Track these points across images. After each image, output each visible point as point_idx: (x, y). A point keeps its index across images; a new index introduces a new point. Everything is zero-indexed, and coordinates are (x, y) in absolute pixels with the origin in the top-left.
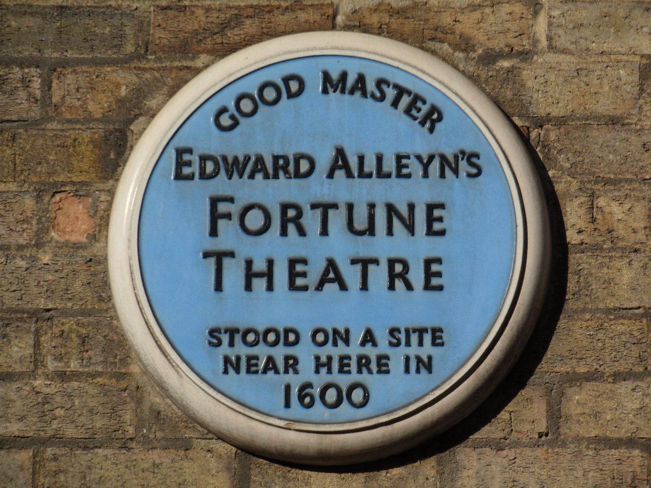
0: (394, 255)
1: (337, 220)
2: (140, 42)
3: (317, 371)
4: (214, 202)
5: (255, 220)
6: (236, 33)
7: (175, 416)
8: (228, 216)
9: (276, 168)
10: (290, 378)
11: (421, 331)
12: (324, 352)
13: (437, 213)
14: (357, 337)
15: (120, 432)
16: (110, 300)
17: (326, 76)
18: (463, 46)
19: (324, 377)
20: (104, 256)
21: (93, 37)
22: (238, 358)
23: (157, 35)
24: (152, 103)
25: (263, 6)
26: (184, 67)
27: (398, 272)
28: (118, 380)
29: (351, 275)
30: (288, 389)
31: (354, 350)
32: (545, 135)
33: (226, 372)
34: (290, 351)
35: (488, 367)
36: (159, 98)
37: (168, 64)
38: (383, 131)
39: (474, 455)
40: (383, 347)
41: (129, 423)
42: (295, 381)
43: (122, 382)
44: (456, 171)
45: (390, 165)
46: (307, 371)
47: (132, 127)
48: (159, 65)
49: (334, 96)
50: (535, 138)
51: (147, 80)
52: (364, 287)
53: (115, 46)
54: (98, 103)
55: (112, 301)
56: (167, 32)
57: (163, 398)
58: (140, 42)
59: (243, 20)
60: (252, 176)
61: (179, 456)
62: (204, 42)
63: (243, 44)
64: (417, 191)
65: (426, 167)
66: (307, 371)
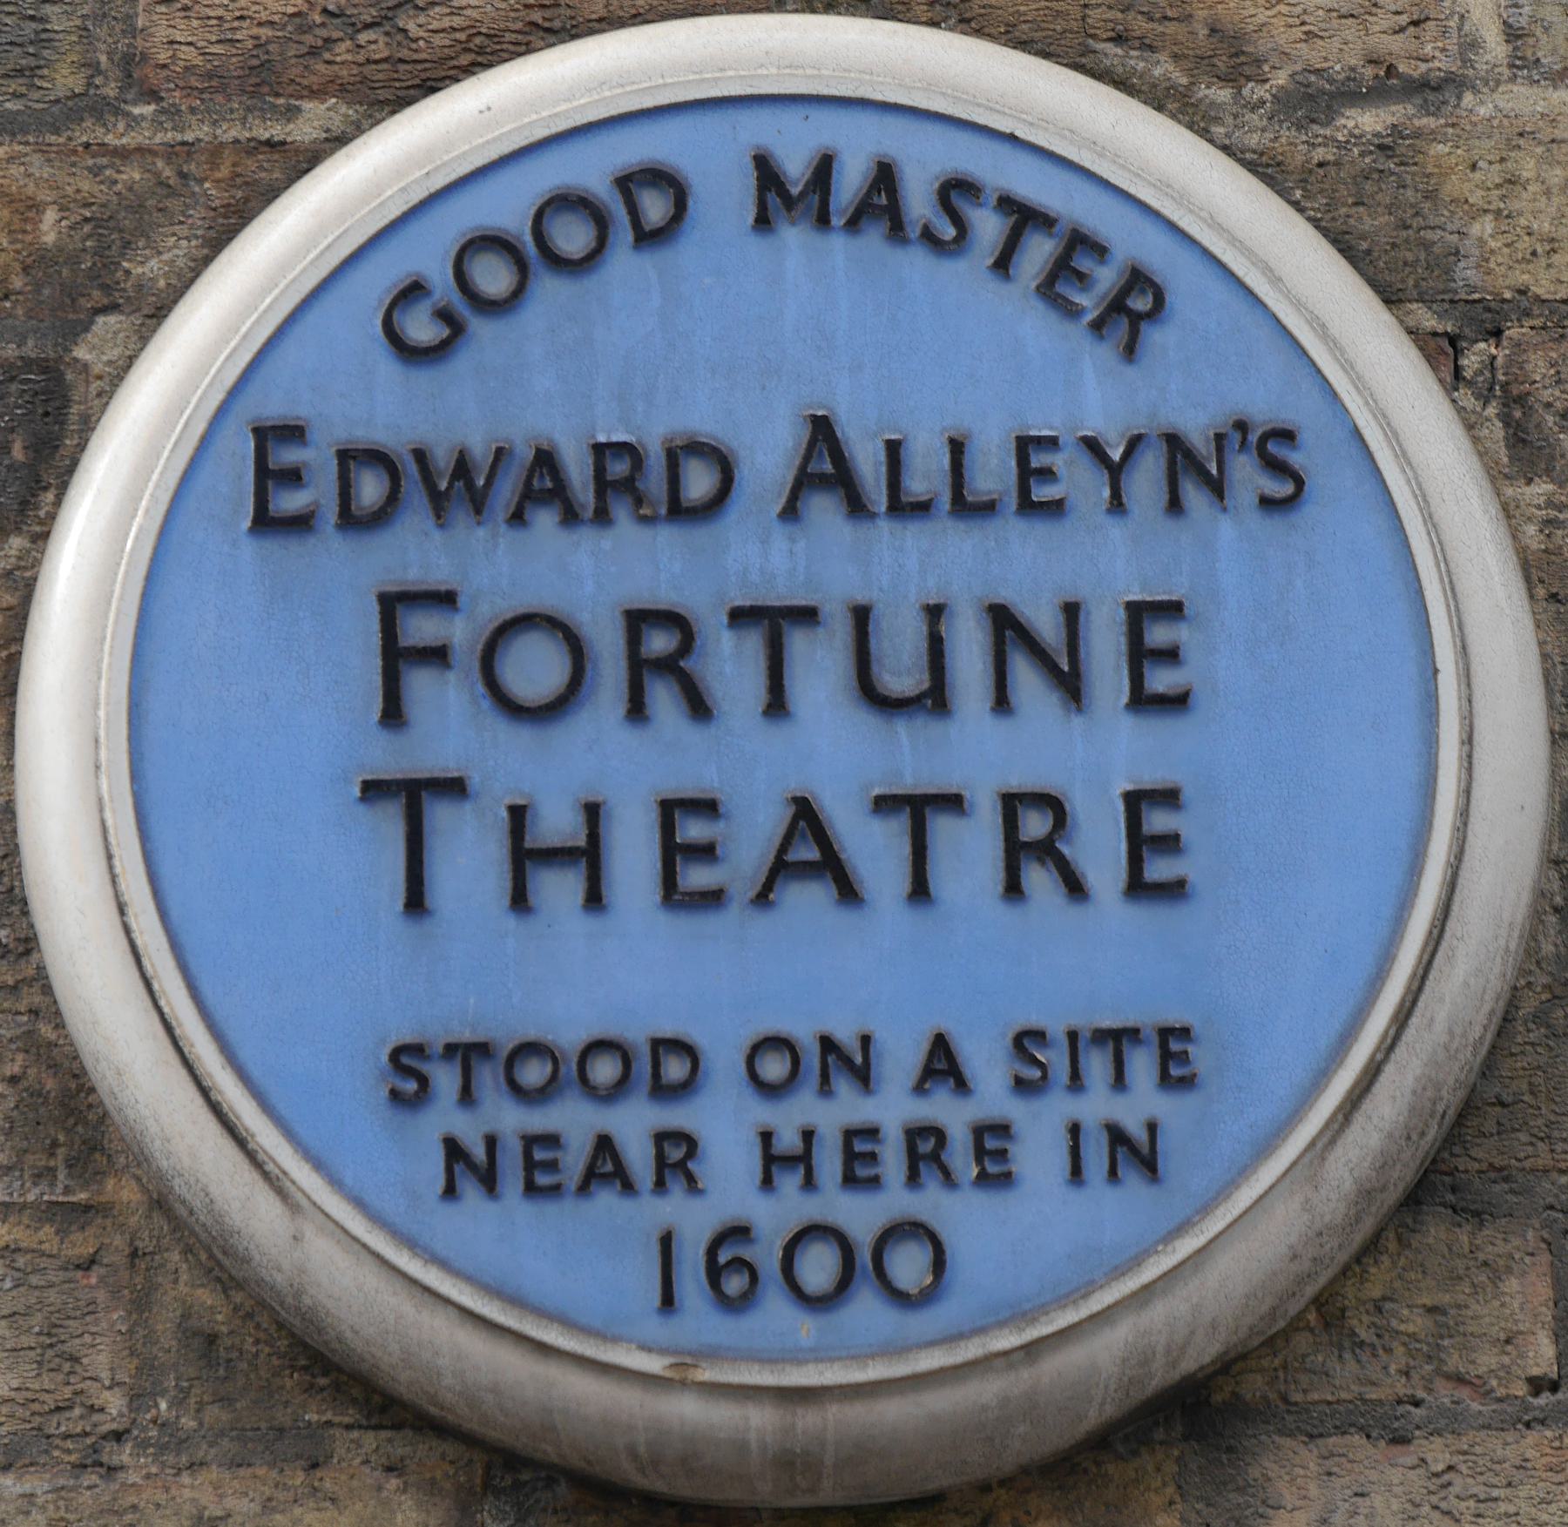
0: (1019, 781)
1: (819, 666)
2: (103, 58)
3: (767, 1182)
4: (392, 604)
5: (535, 668)
6: (435, 25)
7: (267, 1350)
8: (438, 655)
9: (602, 484)
10: (675, 1209)
11: (1118, 1039)
13: (1158, 634)
14: (901, 1057)
15: (77, 1411)
16: (28, 952)
17: (766, 172)
18: (1221, 64)
23: (162, 33)
24: (150, 268)
26: (260, 142)
27: (1034, 838)
29: (875, 850)
31: (893, 1107)
32: (1510, 361)
33: (450, 1191)
34: (675, 1117)
36: (179, 250)
37: (198, 132)
38: (965, 358)
39: (1308, 1457)
40: (992, 1090)
41: (105, 1376)
42: (694, 1221)
43: (77, 1237)
44: (1217, 488)
45: (993, 472)
46: (730, 1183)
47: (81, 353)
49: (794, 236)
50: (1479, 372)
51: (130, 189)
52: (920, 890)
53: (20, 72)
55: (35, 956)
56: (195, 23)
57: (225, 1291)
58: (103, 58)
60: (518, 518)
61: (286, 1487)
62: (327, 56)
63: (465, 60)
64: (1095, 561)
65: (1115, 472)
66: (730, 1183)
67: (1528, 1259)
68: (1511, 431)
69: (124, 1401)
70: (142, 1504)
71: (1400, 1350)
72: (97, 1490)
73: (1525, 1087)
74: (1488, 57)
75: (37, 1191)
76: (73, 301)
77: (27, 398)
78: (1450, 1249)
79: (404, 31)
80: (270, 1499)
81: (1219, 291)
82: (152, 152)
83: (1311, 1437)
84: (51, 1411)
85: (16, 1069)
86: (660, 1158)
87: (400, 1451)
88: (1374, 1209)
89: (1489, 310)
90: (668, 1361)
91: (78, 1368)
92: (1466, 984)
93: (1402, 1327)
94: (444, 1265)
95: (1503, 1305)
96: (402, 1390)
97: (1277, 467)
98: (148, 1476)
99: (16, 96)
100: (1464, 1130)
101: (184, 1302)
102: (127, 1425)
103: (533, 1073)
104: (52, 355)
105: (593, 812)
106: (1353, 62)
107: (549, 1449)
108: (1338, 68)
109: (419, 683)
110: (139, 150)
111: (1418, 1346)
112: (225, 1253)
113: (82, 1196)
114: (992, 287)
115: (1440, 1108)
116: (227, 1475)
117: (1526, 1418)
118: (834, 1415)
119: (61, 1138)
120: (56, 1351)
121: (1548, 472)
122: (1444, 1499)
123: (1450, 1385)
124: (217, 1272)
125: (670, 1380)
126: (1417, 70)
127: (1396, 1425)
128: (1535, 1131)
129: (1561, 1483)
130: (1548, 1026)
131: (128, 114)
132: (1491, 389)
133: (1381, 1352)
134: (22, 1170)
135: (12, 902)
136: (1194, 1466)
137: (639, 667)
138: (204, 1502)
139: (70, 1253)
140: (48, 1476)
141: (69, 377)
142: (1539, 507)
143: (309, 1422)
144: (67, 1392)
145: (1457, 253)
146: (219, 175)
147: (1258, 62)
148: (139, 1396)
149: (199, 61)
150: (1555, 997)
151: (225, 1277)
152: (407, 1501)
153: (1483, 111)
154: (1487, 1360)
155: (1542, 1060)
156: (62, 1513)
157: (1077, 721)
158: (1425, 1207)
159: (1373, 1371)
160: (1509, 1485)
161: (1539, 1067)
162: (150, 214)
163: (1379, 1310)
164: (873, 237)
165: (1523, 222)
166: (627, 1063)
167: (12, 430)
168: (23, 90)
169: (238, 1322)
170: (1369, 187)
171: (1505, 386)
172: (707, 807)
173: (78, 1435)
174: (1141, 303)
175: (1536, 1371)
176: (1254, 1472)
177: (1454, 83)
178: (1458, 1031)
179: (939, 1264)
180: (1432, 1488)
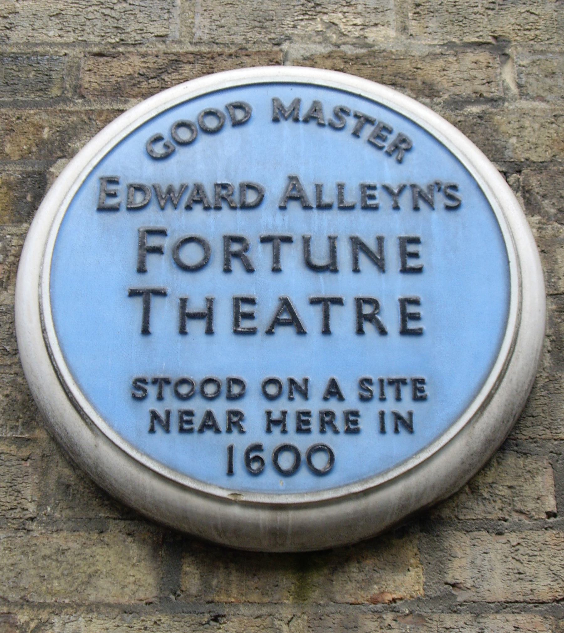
1: (291, 256)
2: (68, 86)
3: (269, 431)
6: (174, 78)
7: (88, 491)
8: (158, 250)
10: (234, 438)
11: (397, 383)
12: (276, 408)
14: (318, 388)
16: (16, 354)
18: (427, 92)
19: (276, 439)
20: (12, 305)
21: (16, 82)
22: (168, 413)
23: (87, 79)
25: (205, 53)
27: (367, 314)
28: (19, 448)
29: (310, 317)
30: (231, 449)
31: (315, 405)
33: (152, 430)
35: (492, 421)
37: (96, 106)
39: (466, 539)
41: (29, 498)
42: (241, 443)
43: (24, 449)
44: (431, 204)
45: (352, 196)
46: (255, 430)
48: (88, 108)
49: (286, 126)
52: (326, 331)
53: (41, 90)
54: (16, 145)
55: (17, 356)
56: (97, 76)
57: (74, 470)
58: (68, 86)
59: (183, 65)
60: (189, 208)
61: (91, 539)
62: (139, 86)
64: (388, 225)
66: (255, 430)
67: (544, 470)
68: (526, 200)
69: (35, 507)
70: (38, 544)
71: (499, 501)
72: (23, 538)
73: (541, 411)
74: (512, 92)
75: (11, 433)
76: (51, 154)
77: (33, 182)
78: (516, 466)
79: (164, 80)
80: (84, 544)
81: (430, 143)
82: (81, 112)
83: (467, 531)
84: (9, 510)
85: (8, 392)
86: (230, 420)
87: (133, 528)
88: (491, 447)
89: (516, 164)
90: (230, 493)
91: (20, 495)
92: (523, 368)
93: (500, 493)
94: (149, 456)
95: (536, 486)
96: (133, 503)
97: (451, 197)
98: (41, 534)
99: (39, 96)
100: (519, 425)
101: (59, 473)
102: (36, 516)
103: (184, 390)
104: (43, 170)
105: (210, 302)
106: (469, 92)
107: (186, 526)
108: (464, 94)
109: (152, 260)
110: (77, 112)
111: (506, 500)
112: (72, 453)
113: (27, 435)
114: (353, 141)
115: (514, 412)
116: (70, 534)
117: (546, 526)
118: (291, 516)
119: (21, 416)
120: (13, 488)
121: (539, 213)
122: (516, 555)
123: (517, 514)
124: (72, 463)
125: (231, 500)
126: (490, 96)
127: (498, 528)
128: (545, 426)
129: (559, 550)
130: (548, 390)
131: (74, 102)
132: (518, 188)
133: (492, 502)
134: (7, 426)
135: (12, 337)
136: (424, 541)
137: (229, 256)
138: (60, 543)
139: (20, 455)
140: (5, 532)
141: (48, 176)
142: (536, 224)
143: (101, 517)
144: (15, 503)
145: (505, 147)
146: (101, 119)
147: (438, 92)
148: (41, 505)
149: (98, 87)
150: (550, 380)
151: (74, 465)
152: (134, 546)
153: (511, 107)
154: (531, 505)
155: (547, 402)
156: (9, 546)
157: (383, 276)
158: (507, 451)
159: (489, 508)
160: (541, 550)
161: (546, 404)
162: (78, 130)
163: (491, 486)
164: (312, 125)
165: (526, 139)
166: (219, 386)
167: (28, 192)
168: (42, 94)
169: (78, 481)
170: (475, 128)
171: (523, 187)
172: (251, 301)
173: (18, 518)
174: (403, 146)
175: (549, 510)
176: (446, 544)
177: (503, 100)
178: (520, 385)
179: (332, 459)
180: (512, 551)
